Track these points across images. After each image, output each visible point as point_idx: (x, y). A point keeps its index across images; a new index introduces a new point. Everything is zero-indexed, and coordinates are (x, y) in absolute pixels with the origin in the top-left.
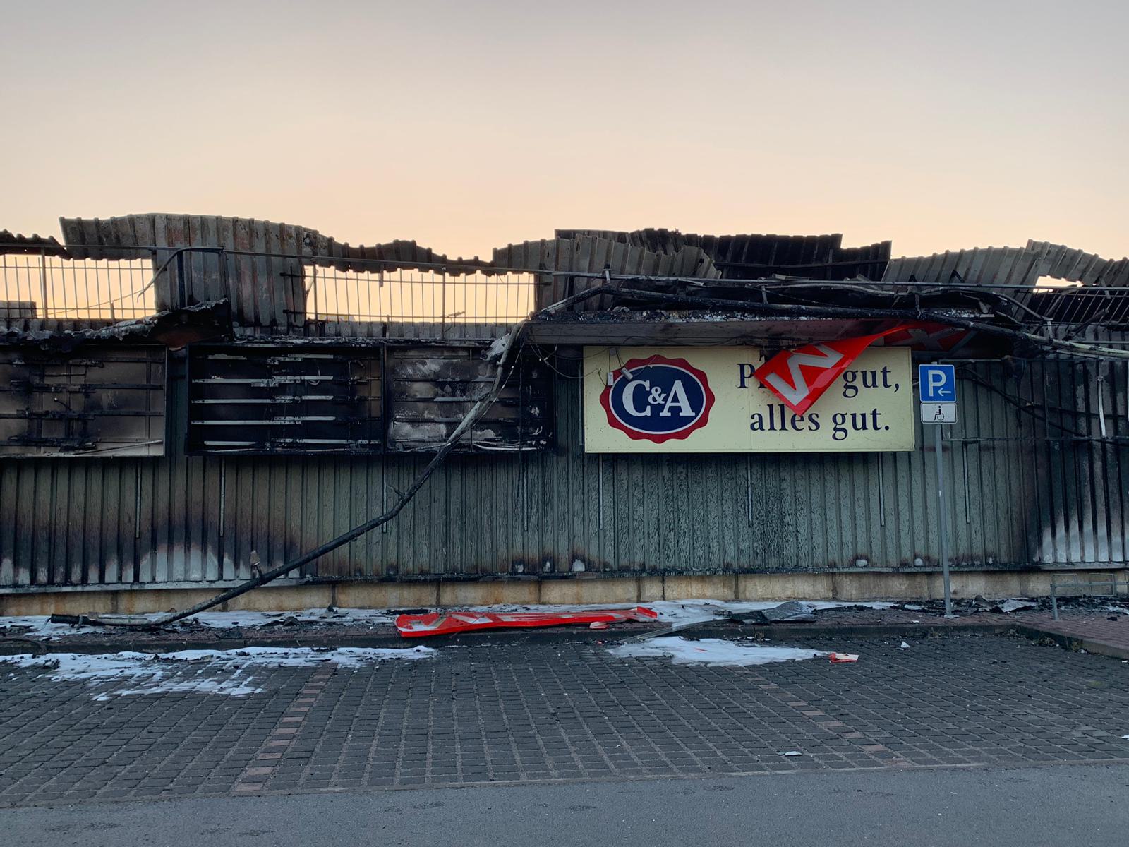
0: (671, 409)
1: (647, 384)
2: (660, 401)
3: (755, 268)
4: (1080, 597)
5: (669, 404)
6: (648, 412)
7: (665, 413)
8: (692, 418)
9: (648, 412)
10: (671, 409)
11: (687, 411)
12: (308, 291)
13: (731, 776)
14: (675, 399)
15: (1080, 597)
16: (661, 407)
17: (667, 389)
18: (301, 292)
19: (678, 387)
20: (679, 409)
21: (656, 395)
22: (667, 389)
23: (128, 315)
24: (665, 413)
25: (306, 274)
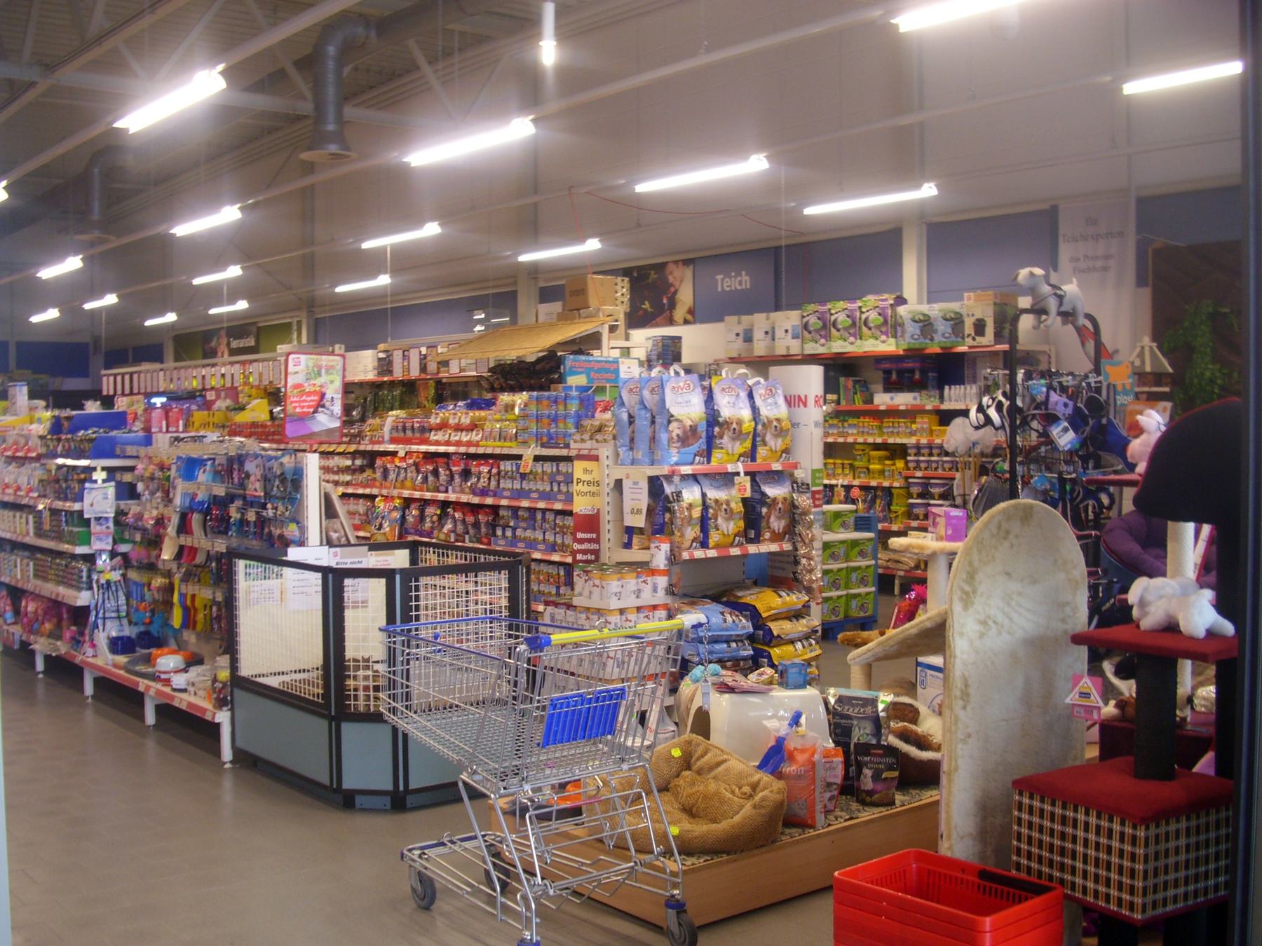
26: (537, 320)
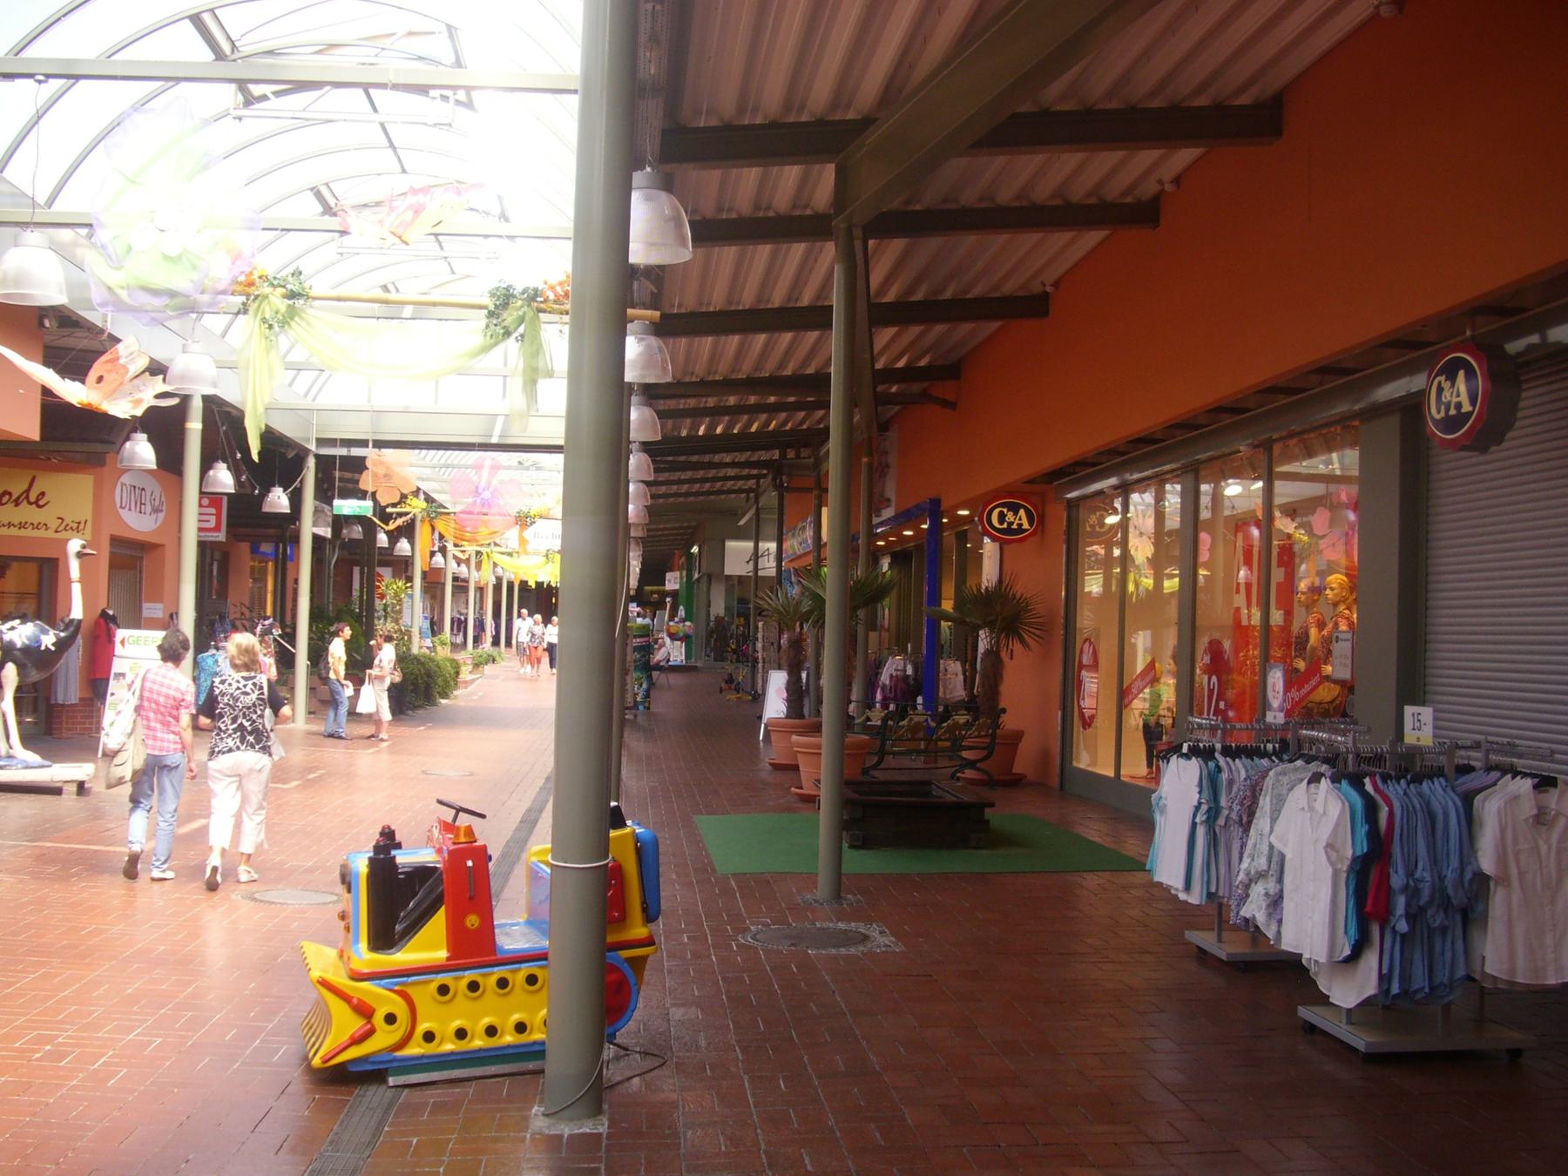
0: (1018, 524)
1: (1005, 510)
2: (1012, 520)
3: (51, 842)
4: (458, 102)
5: (1017, 521)
6: (1005, 526)
7: (1014, 526)
8: (1028, 530)
9: (1005, 526)
10: (1018, 524)
11: (1026, 526)
12: (1205, 652)
13: (718, 1135)
14: (1020, 519)
15: (458, 102)
16: (1012, 523)
17: (1016, 513)
18: (867, 356)
19: (1022, 512)
20: (1022, 525)
21: (1010, 517)
22: (1016, 513)
23: (550, 770)
24: (1014, 526)
25: (116, 653)
26: (575, 92)
